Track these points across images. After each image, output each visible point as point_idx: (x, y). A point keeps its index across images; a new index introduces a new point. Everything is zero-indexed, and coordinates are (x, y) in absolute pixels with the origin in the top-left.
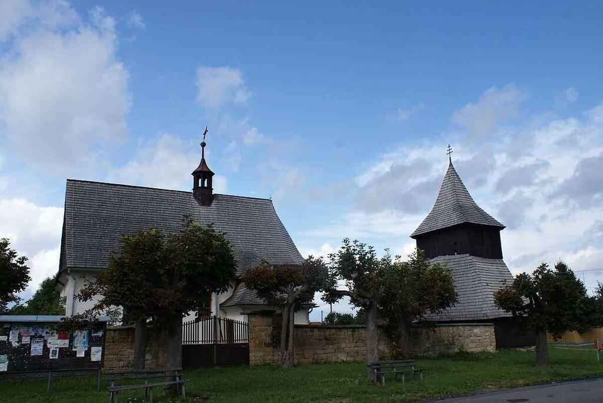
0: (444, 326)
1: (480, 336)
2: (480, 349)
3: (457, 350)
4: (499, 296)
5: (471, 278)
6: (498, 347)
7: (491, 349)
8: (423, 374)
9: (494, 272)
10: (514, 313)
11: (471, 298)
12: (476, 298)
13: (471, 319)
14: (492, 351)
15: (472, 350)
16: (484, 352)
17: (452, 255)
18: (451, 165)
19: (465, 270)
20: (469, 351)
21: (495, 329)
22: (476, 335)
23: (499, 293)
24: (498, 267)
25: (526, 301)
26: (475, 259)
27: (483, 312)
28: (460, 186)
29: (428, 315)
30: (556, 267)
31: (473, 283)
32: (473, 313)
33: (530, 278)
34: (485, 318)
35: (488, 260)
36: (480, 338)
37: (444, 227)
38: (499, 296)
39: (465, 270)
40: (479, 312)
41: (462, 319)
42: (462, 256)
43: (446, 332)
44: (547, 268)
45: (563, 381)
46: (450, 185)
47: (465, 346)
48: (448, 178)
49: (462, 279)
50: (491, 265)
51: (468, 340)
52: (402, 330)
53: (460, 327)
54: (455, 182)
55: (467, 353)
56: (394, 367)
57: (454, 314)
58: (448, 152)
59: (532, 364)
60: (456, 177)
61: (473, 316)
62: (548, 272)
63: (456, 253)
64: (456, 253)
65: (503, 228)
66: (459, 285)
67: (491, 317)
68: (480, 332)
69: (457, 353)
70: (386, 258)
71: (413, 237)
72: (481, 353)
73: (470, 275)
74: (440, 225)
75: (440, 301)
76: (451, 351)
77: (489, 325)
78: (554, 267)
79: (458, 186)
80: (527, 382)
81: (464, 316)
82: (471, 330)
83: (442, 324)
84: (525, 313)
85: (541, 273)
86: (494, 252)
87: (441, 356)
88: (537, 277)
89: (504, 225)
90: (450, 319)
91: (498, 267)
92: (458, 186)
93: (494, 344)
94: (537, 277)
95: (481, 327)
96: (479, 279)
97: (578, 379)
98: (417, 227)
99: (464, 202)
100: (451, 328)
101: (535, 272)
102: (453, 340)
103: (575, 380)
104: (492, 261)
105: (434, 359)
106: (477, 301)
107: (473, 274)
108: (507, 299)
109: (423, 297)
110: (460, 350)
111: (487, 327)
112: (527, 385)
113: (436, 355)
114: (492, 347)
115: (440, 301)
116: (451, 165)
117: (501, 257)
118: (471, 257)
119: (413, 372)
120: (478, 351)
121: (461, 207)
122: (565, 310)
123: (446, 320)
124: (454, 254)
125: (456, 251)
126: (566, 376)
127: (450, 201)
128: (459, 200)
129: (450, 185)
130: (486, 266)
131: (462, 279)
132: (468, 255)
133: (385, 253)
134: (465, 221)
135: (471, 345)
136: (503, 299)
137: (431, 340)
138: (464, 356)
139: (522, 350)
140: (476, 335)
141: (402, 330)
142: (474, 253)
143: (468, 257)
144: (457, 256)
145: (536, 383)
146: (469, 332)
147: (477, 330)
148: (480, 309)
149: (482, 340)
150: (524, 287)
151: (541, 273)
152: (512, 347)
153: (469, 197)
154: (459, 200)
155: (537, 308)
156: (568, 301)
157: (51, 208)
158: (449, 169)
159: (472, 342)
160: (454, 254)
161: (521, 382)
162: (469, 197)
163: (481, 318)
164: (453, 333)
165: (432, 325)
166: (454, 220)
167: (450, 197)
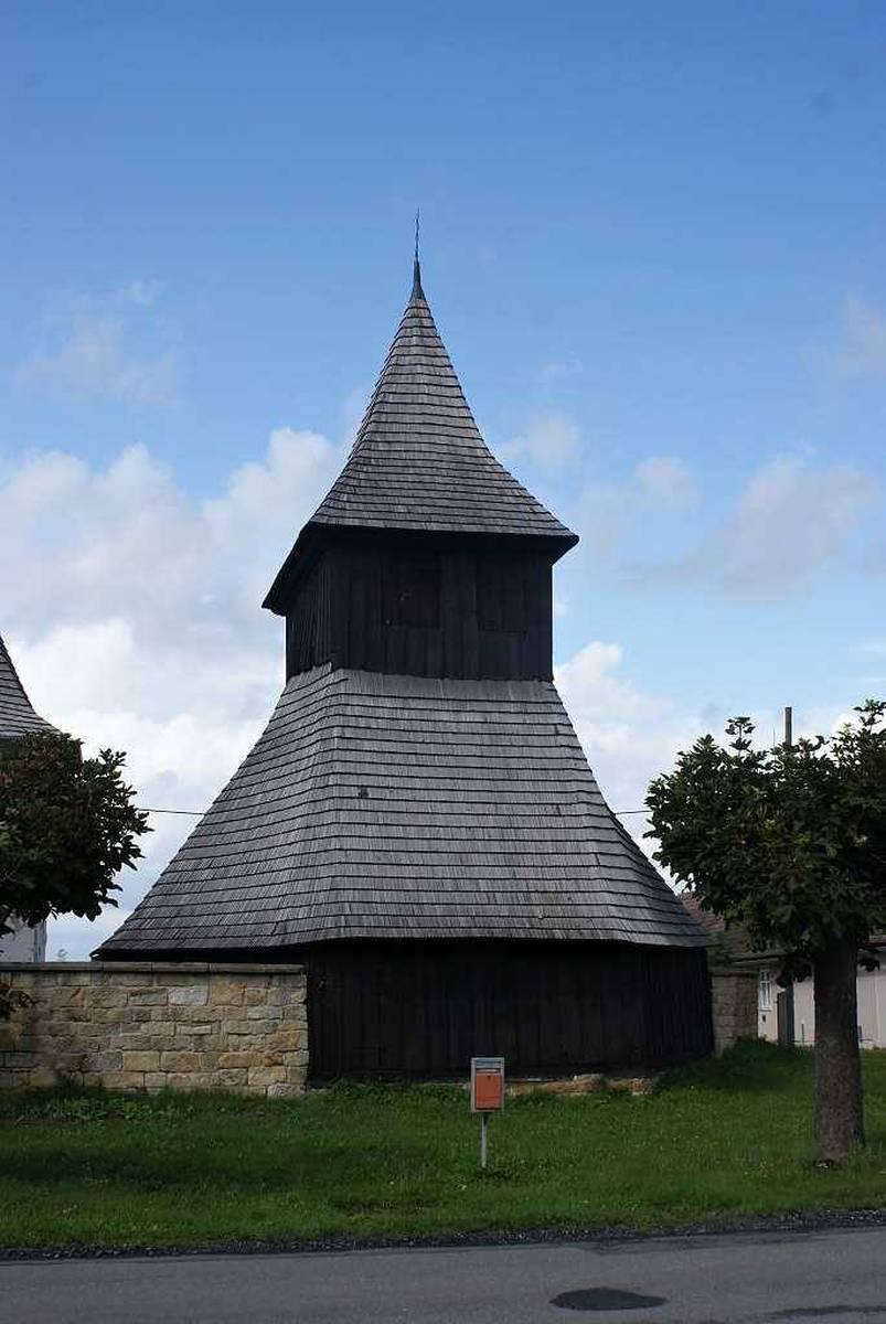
6: (316, 1073)
15: (138, 1079)
18: (419, 293)
47: (99, 1061)
83: (200, 966)
110: (58, 1073)
114: (278, 1073)
117: (538, 665)
118: (341, 673)
146: (139, 1000)
159: (149, 1044)
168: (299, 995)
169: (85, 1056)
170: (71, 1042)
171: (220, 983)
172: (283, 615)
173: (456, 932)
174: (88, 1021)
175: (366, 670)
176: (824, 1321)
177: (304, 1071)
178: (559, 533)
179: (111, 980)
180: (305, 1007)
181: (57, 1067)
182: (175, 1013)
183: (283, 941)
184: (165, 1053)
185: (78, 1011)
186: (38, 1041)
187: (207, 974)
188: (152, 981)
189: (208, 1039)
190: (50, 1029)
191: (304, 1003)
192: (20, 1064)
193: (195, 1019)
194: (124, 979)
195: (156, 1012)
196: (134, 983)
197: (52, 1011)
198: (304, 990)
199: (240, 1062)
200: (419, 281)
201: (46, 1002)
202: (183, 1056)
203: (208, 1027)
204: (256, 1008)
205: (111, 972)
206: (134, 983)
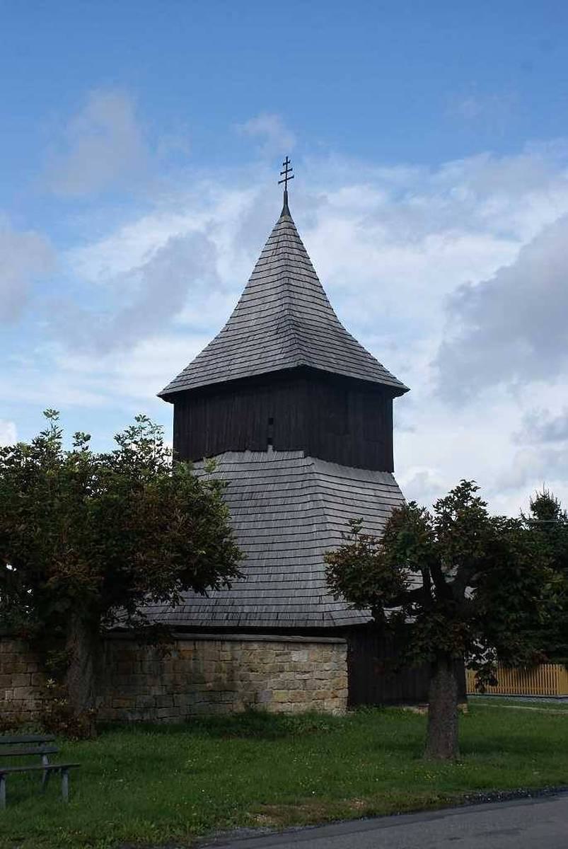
0: (208, 640)
1: (306, 672)
2: (304, 707)
3: (241, 708)
4: (341, 561)
5: (302, 515)
6: (352, 702)
7: (335, 707)
8: (71, 780)
9: (367, 505)
10: (377, 612)
11: (296, 569)
12: (310, 568)
13: (288, 625)
14: (335, 712)
15: (280, 707)
16: (312, 715)
17: (259, 451)
18: (286, 212)
19: (290, 493)
20: (273, 709)
21: (350, 654)
22: (294, 669)
23: (342, 554)
24: (379, 493)
25: (416, 581)
26: (318, 467)
27: (321, 608)
28: (304, 272)
29: (157, 611)
30: (533, 508)
31: (306, 529)
32: (298, 609)
33: (427, 517)
34: (326, 624)
35: (353, 473)
36: (306, 676)
37: (246, 375)
38: (341, 561)
39: (290, 493)
40: (311, 608)
41: (265, 624)
42: (285, 455)
43: (212, 658)
44: (473, 494)
45: (476, 801)
46: (277, 264)
47: (263, 697)
48: (273, 246)
49: (280, 516)
50: (361, 485)
51: (271, 682)
52: (77, 647)
53: (255, 646)
54: (292, 257)
55: (265, 716)
56: (42, 754)
57: (247, 609)
58: (283, 177)
59: (414, 749)
60: (294, 245)
61: (295, 616)
62: (474, 505)
63: (271, 447)
64: (271, 447)
65: (401, 391)
66: (242, 526)
67: (341, 623)
68: (308, 659)
69: (241, 715)
70: (46, 438)
71: (166, 397)
72: (301, 717)
73: (300, 507)
74: (240, 367)
75: (178, 568)
76: (223, 710)
77: (333, 644)
78: (529, 506)
79: (298, 270)
80: (372, 806)
81: (273, 617)
82: (287, 654)
83: (189, 635)
84: (412, 613)
85: (458, 505)
86: (378, 457)
87: (192, 724)
88: (447, 516)
89: (406, 385)
90: (232, 624)
91: (379, 493)
92: (298, 270)
93: (344, 693)
94: (447, 516)
95: (313, 647)
96: (320, 520)
97: (516, 796)
98: (180, 371)
99: (309, 314)
100: (227, 647)
101: (444, 503)
102: (231, 679)
103: (505, 798)
104: (364, 474)
105: (176, 729)
106: (311, 576)
107: (308, 506)
108: (358, 574)
109: (133, 553)
110: (246, 706)
111: (329, 647)
112: (370, 814)
113: (176, 721)
114: (336, 702)
115: (178, 568)
116: (286, 212)
117: (390, 469)
118: (309, 460)
119: (45, 772)
120: (295, 711)
121: (296, 325)
122: (512, 608)
123: (226, 624)
124: (266, 451)
125: (270, 442)
126: (484, 786)
127: (273, 307)
128: (293, 308)
129: (277, 264)
130: (346, 488)
131: (280, 516)
132: (301, 454)
133: (46, 424)
134: (301, 362)
135: (281, 695)
136: (350, 574)
137: (168, 677)
138: (260, 725)
139: (416, 710)
140: (294, 669)
141: (77, 647)
142: (316, 451)
143: (299, 461)
144: (271, 455)
145: (417, 809)
146: (279, 659)
147: (300, 656)
148: (316, 600)
149: (311, 681)
150: (409, 540)
151: (458, 505)
152: (391, 702)
153: (329, 311)
154: (293, 308)
155: (440, 600)
156: (520, 585)
157: (236, 456)
158: (279, 223)
159: (284, 686)
160: (266, 451)
161: (359, 804)
162: (329, 311)
163: (316, 624)
164: (233, 659)
165: (161, 634)
166: (272, 357)
167: (273, 298)
168: (344, 656)
169: (257, 693)
170: (250, 684)
171: (313, 648)
172: (172, 403)
173: (366, 619)
174: (257, 672)
175: (319, 458)
176: (248, 846)
177: (346, 700)
178: (397, 385)
179: (268, 646)
180: (346, 663)
181: (244, 700)
182: (295, 667)
183: (202, 623)
184: (291, 691)
185: (253, 666)
186: (235, 684)
187: (305, 643)
188: (284, 648)
189: (308, 682)
190: (240, 676)
191: (346, 661)
192: (228, 699)
193: (303, 671)
194: (273, 646)
195: (286, 667)
196: (277, 648)
197: (240, 665)
198: (346, 653)
199: (321, 697)
200: (287, 204)
201: (237, 660)
202: (298, 693)
203: (308, 675)
204: (327, 664)
205: (198, 640)
206: (277, 648)
